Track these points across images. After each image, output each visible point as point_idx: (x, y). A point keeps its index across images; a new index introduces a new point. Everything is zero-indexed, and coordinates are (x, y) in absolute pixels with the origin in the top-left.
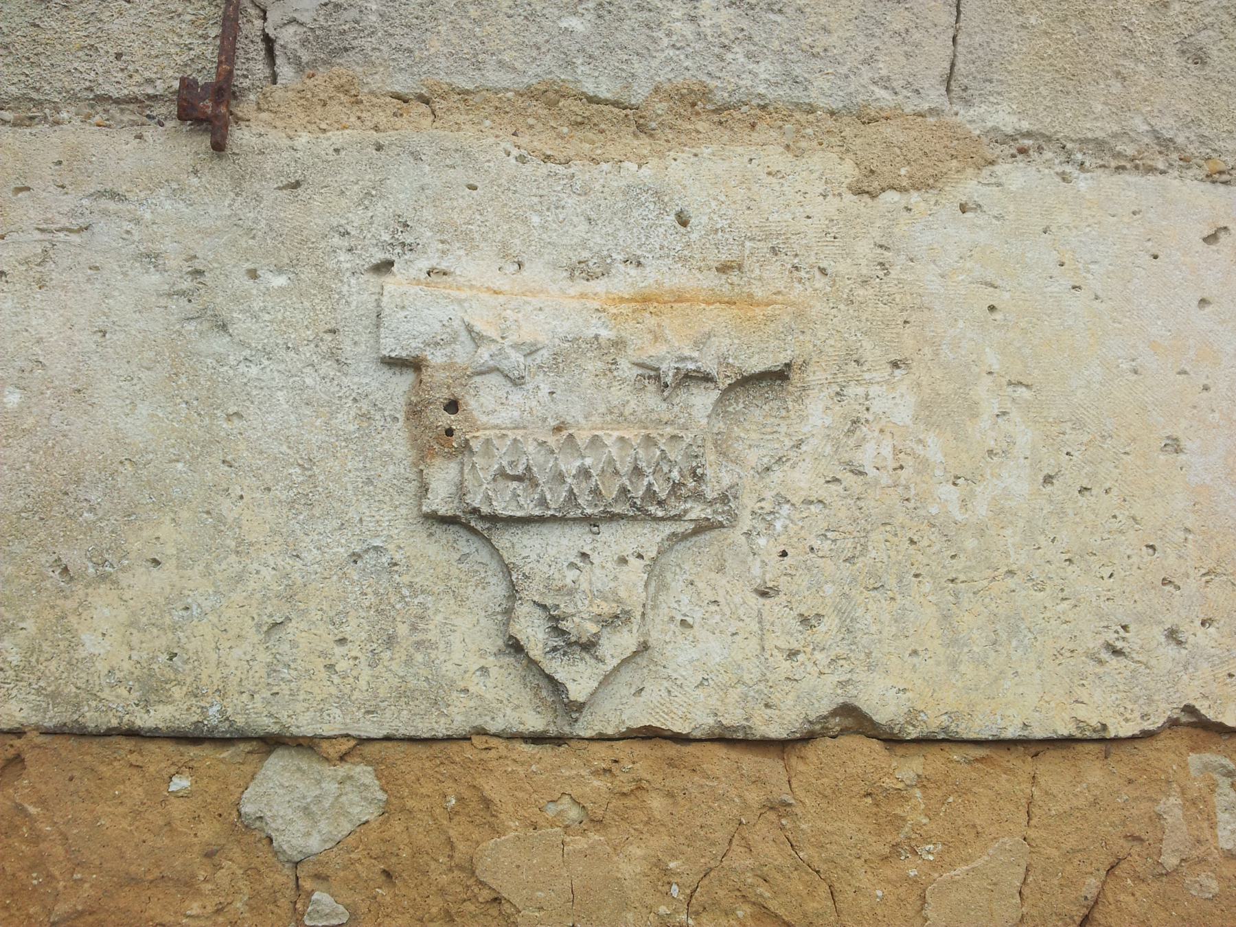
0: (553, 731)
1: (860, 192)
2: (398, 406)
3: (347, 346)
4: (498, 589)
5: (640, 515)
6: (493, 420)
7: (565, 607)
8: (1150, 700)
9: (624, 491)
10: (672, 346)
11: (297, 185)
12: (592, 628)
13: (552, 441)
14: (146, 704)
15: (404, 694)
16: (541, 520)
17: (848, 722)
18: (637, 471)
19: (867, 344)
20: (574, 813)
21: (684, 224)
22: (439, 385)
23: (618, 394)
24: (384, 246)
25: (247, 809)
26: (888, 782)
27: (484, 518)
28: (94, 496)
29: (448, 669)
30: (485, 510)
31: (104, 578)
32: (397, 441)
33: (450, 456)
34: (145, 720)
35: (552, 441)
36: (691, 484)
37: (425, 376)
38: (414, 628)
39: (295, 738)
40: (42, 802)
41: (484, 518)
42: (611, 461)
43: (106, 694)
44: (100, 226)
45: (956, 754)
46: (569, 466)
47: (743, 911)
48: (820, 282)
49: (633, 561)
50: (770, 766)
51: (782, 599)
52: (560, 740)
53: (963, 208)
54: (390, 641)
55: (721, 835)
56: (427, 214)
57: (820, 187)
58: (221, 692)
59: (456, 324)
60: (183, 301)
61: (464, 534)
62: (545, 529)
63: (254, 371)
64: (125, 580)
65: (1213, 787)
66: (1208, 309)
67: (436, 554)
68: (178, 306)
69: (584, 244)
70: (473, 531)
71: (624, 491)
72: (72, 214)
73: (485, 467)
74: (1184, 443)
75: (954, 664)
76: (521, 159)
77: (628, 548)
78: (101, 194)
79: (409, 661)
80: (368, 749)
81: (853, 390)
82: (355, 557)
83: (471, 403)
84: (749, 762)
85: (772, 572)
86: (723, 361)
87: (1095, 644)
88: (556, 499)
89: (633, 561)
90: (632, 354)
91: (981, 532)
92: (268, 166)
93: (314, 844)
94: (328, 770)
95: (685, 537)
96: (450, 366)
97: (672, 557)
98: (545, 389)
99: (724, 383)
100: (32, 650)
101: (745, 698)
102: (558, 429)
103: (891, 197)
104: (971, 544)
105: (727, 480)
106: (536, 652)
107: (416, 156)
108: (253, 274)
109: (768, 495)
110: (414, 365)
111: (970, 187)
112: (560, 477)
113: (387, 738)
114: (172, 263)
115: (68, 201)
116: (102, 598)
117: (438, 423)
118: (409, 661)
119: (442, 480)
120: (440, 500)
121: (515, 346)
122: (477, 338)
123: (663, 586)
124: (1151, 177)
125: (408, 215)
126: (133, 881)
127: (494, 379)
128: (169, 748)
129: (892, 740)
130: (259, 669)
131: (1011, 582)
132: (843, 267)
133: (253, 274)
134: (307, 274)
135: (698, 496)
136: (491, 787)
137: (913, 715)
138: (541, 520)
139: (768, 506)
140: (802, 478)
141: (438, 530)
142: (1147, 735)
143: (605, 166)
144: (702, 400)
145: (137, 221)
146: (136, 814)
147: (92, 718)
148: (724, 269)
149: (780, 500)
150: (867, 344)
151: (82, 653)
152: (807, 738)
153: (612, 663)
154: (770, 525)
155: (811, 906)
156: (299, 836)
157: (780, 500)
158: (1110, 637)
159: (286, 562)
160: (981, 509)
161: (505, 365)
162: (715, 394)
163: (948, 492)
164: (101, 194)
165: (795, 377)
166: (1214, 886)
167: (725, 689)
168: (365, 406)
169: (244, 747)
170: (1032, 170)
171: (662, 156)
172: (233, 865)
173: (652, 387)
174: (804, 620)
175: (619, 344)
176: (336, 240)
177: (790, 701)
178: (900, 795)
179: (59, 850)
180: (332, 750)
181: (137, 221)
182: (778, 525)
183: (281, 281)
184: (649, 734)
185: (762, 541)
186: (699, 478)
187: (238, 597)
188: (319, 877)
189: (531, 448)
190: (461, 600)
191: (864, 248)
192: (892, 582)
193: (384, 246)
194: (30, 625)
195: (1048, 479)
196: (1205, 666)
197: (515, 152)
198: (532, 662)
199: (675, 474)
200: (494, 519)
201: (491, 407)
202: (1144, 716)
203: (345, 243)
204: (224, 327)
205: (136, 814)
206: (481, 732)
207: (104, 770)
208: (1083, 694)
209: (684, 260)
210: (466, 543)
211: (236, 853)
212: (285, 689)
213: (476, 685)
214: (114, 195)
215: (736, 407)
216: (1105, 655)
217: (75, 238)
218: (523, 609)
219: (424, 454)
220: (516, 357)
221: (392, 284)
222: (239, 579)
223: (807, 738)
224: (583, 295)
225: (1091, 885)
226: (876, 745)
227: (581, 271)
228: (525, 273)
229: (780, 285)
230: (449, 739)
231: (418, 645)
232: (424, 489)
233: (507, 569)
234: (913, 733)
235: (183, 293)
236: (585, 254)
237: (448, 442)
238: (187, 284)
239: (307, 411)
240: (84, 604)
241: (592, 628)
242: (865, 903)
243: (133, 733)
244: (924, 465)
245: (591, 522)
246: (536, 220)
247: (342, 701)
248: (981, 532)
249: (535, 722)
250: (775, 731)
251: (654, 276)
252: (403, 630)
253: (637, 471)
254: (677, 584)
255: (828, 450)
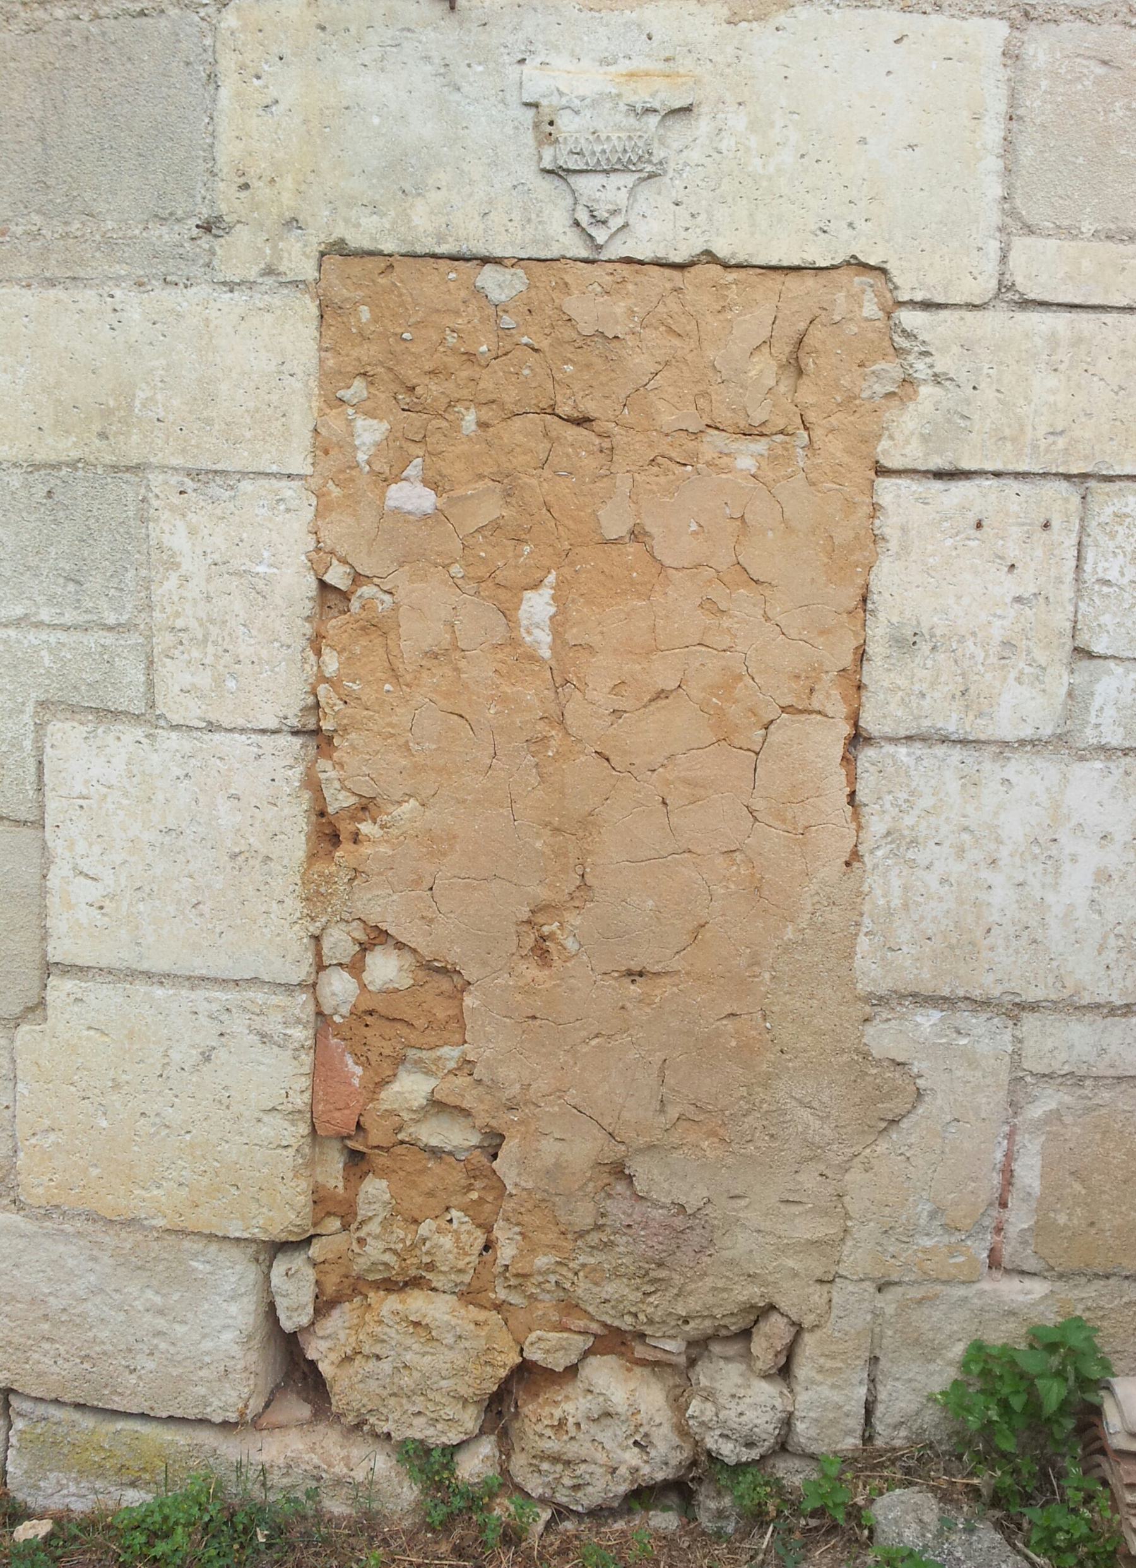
0: (591, 257)
1: (730, 23)
2: (529, 123)
3: (508, 97)
4: (570, 201)
5: (626, 170)
6: (568, 129)
7: (596, 206)
8: (836, 252)
9: (619, 159)
10: (641, 96)
11: (485, 24)
12: (607, 215)
13: (591, 138)
14: (439, 244)
15: (534, 241)
16: (587, 171)
17: (709, 259)
18: (625, 151)
19: (728, 94)
20: (599, 289)
21: (650, 39)
22: (546, 112)
23: (619, 117)
24: (522, 52)
25: (477, 284)
26: (722, 281)
27: (564, 170)
28: (413, 161)
29: (551, 233)
30: (565, 167)
31: (419, 194)
32: (529, 138)
33: (551, 144)
34: (438, 250)
35: (591, 138)
36: (647, 156)
37: (540, 109)
38: (538, 216)
39: (495, 258)
40: (402, 281)
41: (564, 170)
42: (614, 146)
43: (423, 240)
44: (405, 44)
45: (751, 271)
46: (598, 148)
47: (662, 329)
48: (709, 65)
49: (623, 188)
50: (675, 274)
51: (684, 206)
52: (593, 262)
53: (777, 29)
54: (529, 221)
55: (655, 300)
56: (540, 37)
57: (711, 21)
58: (467, 240)
59: (553, 87)
60: (442, 78)
61: (557, 178)
62: (588, 175)
63: (472, 108)
64: (428, 195)
65: (863, 292)
66: (891, 76)
67: (547, 185)
68: (440, 79)
69: (606, 50)
70: (560, 176)
71: (619, 159)
72: (392, 38)
73: (564, 149)
74: (868, 140)
75: (753, 234)
76: (580, 10)
77: (621, 184)
78: (403, 29)
79: (536, 229)
80: (522, 263)
81: (720, 116)
82: (515, 187)
83: (559, 122)
84: (667, 272)
85: (680, 196)
86: (663, 103)
87: (814, 227)
88: (592, 162)
89: (623, 188)
90: (625, 100)
91: (770, 179)
92: (473, 16)
93: (503, 298)
94: (507, 270)
95: (645, 179)
96: (550, 106)
97: (639, 188)
98: (589, 115)
99: (663, 113)
100: (394, 223)
101: (666, 246)
102: (594, 133)
103: (744, 24)
104: (765, 184)
105: (662, 155)
106: (584, 225)
107: (535, 10)
108: (469, 66)
109: (681, 162)
110: (536, 105)
111: (781, 19)
112: (593, 153)
113: (529, 259)
114: (437, 61)
115: (390, 33)
116: (419, 202)
117: (546, 130)
118: (536, 229)
119: (548, 154)
120: (547, 164)
121: (577, 97)
122: (561, 94)
123: (635, 200)
124: (872, 10)
125: (532, 38)
126: (438, 311)
127: (568, 111)
128: (448, 262)
129: (726, 266)
130: (481, 231)
131: (781, 201)
132: (719, 59)
133: (469, 66)
134: (492, 65)
135: (650, 162)
136: (567, 278)
137: (734, 254)
138: (587, 171)
139: (680, 167)
140: (695, 155)
141: (545, 175)
142: (834, 267)
143: (616, 12)
144: (653, 120)
145: (420, 42)
146: (436, 287)
147: (419, 250)
148: (667, 60)
149: (686, 164)
150: (728, 94)
151: (413, 224)
152: (692, 264)
153: (614, 230)
154: (681, 175)
155: (688, 328)
156: (497, 295)
157: (686, 164)
158: (822, 225)
159: (488, 189)
160: (771, 169)
161: (572, 105)
162: (659, 118)
163: (758, 162)
164: (403, 29)
165: (695, 110)
166: (856, 330)
167: (659, 242)
168: (516, 123)
169: (476, 262)
170: (812, 9)
171: (641, 7)
172: (473, 306)
173: (632, 114)
174: (693, 216)
175: (619, 95)
176: (502, 49)
177: (684, 247)
178: (727, 287)
179: (410, 299)
180: (508, 263)
181: (420, 42)
182: (685, 175)
183: (480, 68)
184: (628, 261)
185: (677, 182)
186: (650, 154)
187: (471, 202)
188: (506, 311)
189: (583, 141)
190: (556, 205)
191: (730, 50)
192: (730, 200)
193: (522, 52)
194: (392, 213)
195: (802, 156)
196: (864, 239)
197: (577, 7)
198: (583, 229)
199: (640, 152)
200: (568, 171)
201: (567, 124)
202: (833, 259)
203: (506, 51)
204: (459, 89)
205: (436, 287)
206: (564, 257)
207: (423, 270)
208: (806, 248)
209: (649, 56)
210: (557, 182)
211: (474, 301)
212: (490, 238)
213: (562, 239)
214: (409, 30)
215: (669, 123)
216: (818, 232)
217: (394, 49)
218: (579, 208)
219: (540, 143)
220: (577, 102)
221: (526, 68)
222: (471, 195)
223: (692, 264)
224: (605, 73)
225: (802, 326)
226: (719, 267)
227: (605, 62)
228: (581, 63)
229: (691, 68)
230: (552, 260)
231: (540, 222)
232: (541, 158)
233: (573, 192)
234: (733, 262)
235: (440, 74)
236: (607, 54)
237: (550, 139)
238: (442, 70)
239: (493, 125)
240: (412, 206)
241: (607, 215)
242: (709, 328)
243: (434, 256)
244: (748, 149)
245: (606, 172)
246: (586, 38)
247: (512, 243)
248: (770, 179)
249: (584, 254)
250: (678, 260)
251: (639, 63)
252: (533, 216)
253: (625, 151)
254: (641, 199)
255: (708, 142)
